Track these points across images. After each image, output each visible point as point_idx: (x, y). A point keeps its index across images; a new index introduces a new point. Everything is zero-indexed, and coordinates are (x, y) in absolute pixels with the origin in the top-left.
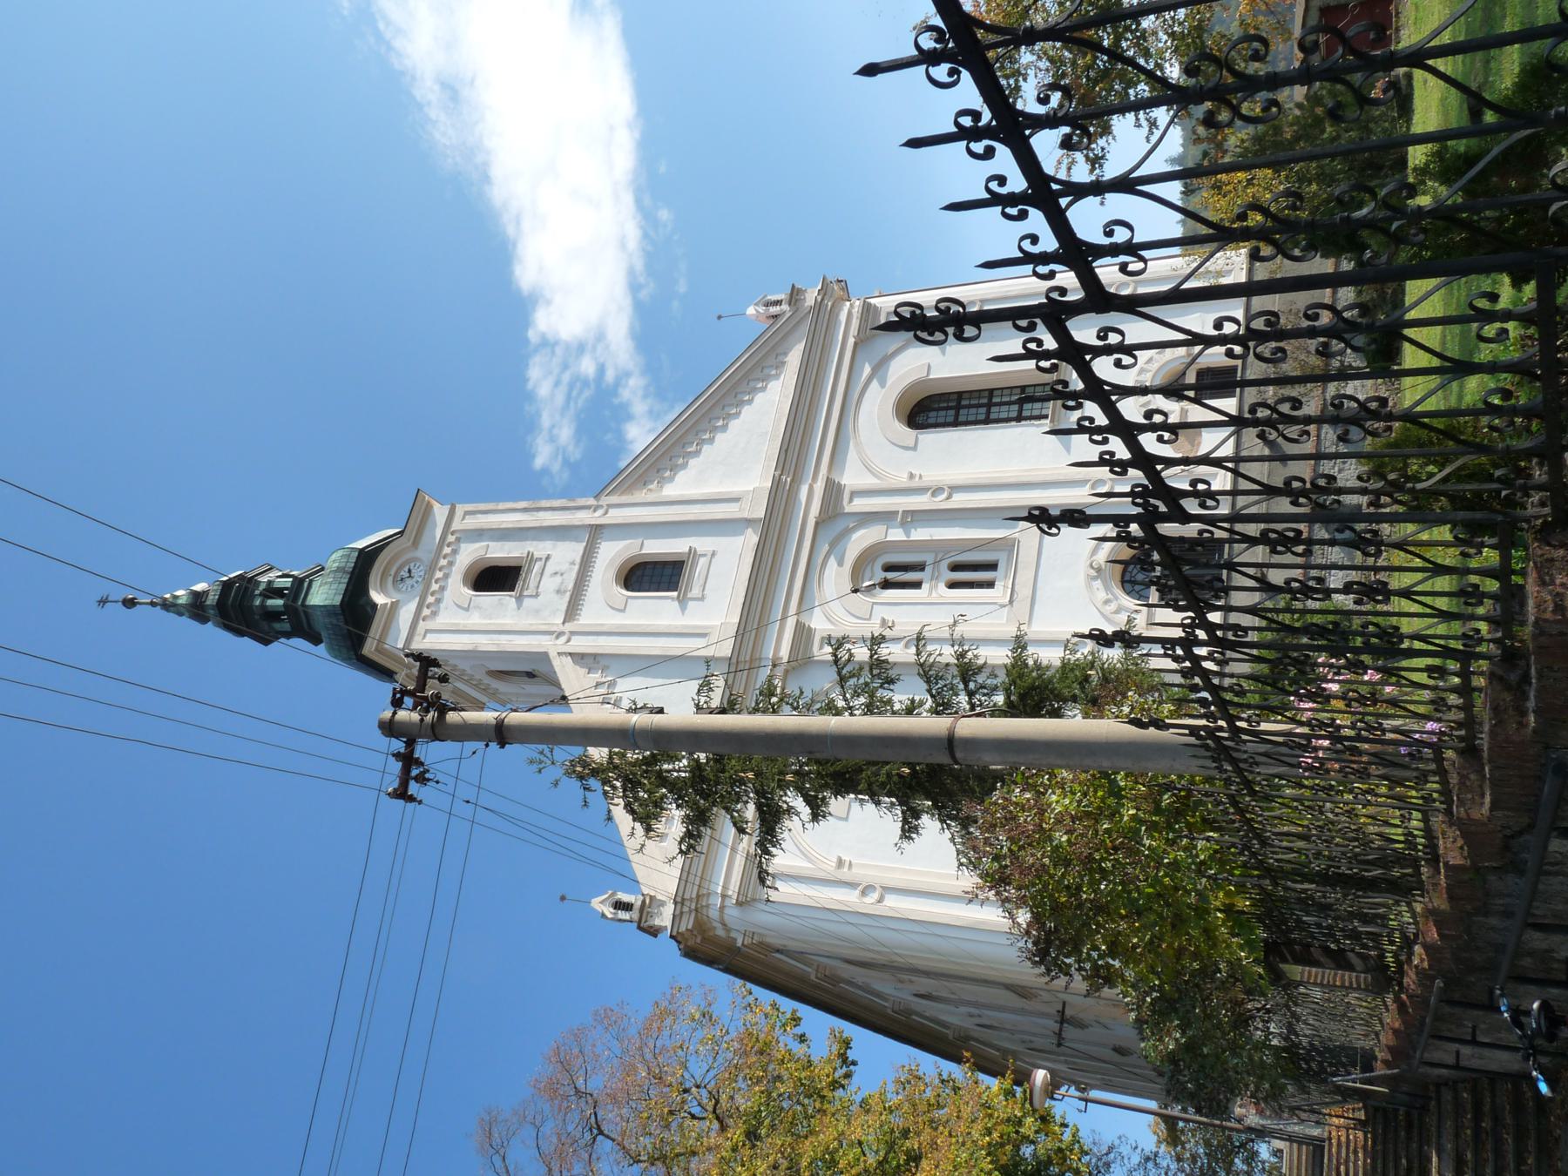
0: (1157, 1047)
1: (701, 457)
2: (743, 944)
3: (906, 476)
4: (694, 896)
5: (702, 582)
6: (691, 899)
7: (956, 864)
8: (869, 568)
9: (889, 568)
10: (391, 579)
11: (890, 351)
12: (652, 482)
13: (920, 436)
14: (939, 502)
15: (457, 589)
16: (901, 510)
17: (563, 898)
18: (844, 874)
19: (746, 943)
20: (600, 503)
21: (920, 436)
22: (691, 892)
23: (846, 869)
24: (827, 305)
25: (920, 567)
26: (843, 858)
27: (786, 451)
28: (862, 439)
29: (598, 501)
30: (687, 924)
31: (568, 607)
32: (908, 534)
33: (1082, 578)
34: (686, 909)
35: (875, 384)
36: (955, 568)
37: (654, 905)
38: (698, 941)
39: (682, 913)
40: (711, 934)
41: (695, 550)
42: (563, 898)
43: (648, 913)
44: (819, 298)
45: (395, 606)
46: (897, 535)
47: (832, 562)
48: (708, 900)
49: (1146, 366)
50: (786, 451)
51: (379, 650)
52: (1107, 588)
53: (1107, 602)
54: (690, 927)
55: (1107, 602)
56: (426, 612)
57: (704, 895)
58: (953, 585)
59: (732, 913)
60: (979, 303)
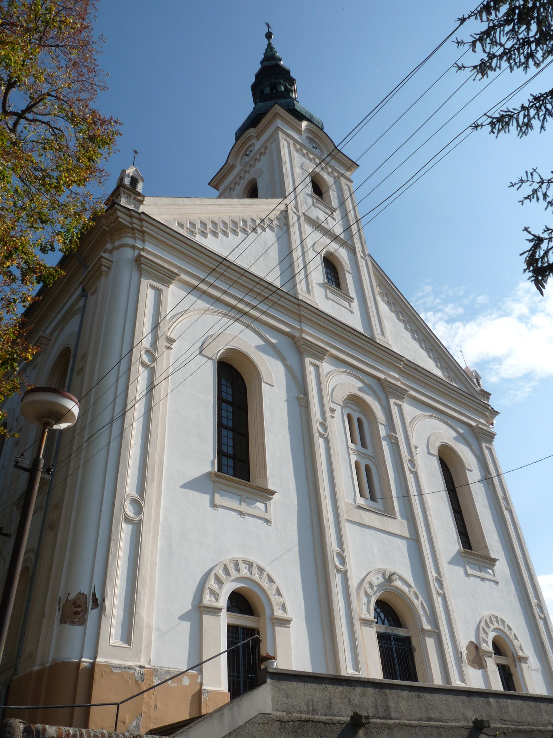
0: (55, 203)
1: (397, 321)
2: (102, 257)
3: (417, 444)
4: (144, 229)
5: (336, 301)
6: (142, 226)
7: (549, 227)
8: (358, 409)
9: (359, 421)
10: (312, 137)
11: (473, 447)
12: (380, 289)
13: (435, 458)
14: (407, 466)
15: (311, 167)
16: (397, 436)
17: (136, 152)
18: (162, 343)
19: (103, 267)
20: (367, 256)
21: (435, 458)
22: (147, 228)
23: (166, 344)
24: (487, 412)
25: (364, 445)
26: (174, 344)
27: (416, 369)
28: (427, 420)
29: (367, 255)
30: (123, 218)
31: (310, 218)
32: (384, 438)
33: (382, 566)
34: (134, 220)
35: (455, 434)
36: (367, 468)
37: (137, 203)
38: (105, 227)
39: (131, 216)
40: (108, 240)
41: (352, 302)
42: (136, 152)
43: (130, 196)
44: (490, 408)
45: (299, 132)
46: (383, 431)
47: (360, 385)
48: (139, 239)
49: (265, 575)
50: (416, 369)
51: (276, 115)
52: (380, 586)
53: (371, 585)
54: (120, 219)
55: (371, 585)
56: (298, 147)
57: (144, 237)
58: (357, 463)
59: (129, 254)
60: (137, 519)
